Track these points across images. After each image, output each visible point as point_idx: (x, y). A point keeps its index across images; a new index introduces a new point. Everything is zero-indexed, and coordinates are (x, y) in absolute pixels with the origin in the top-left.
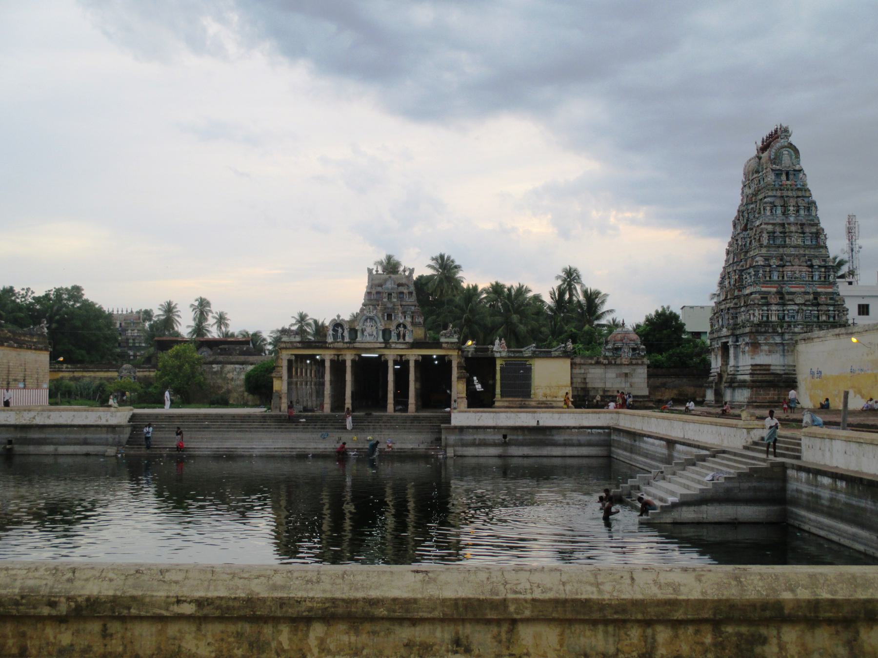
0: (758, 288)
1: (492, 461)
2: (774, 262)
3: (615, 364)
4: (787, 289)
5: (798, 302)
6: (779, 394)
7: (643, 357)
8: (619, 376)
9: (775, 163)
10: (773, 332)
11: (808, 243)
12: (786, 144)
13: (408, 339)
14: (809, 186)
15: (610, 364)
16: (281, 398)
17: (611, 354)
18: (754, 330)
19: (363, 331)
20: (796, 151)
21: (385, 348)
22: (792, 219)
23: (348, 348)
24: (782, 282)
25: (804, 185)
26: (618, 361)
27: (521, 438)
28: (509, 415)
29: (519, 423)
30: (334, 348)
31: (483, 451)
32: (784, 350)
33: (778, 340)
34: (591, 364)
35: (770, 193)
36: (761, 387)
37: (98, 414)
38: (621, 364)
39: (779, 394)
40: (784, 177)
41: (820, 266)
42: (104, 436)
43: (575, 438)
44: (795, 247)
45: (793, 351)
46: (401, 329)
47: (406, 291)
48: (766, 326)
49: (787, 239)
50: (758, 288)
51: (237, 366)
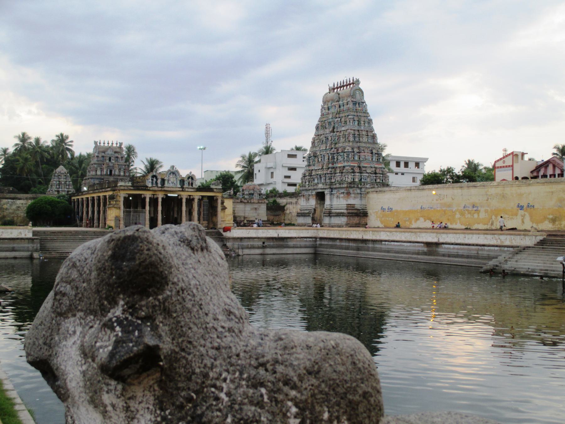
0: (349, 164)
2: (356, 150)
4: (362, 165)
11: (370, 141)
15: (248, 202)
19: (168, 181)
20: (362, 92)
21: (182, 191)
22: (362, 128)
23: (161, 191)
25: (366, 110)
26: (252, 201)
27: (272, 243)
28: (263, 231)
32: (361, 197)
33: (359, 191)
34: (238, 202)
36: (352, 216)
37: (20, 230)
40: (357, 105)
42: (26, 245)
43: (298, 243)
46: (190, 180)
47: (119, 156)
51: (10, 200)
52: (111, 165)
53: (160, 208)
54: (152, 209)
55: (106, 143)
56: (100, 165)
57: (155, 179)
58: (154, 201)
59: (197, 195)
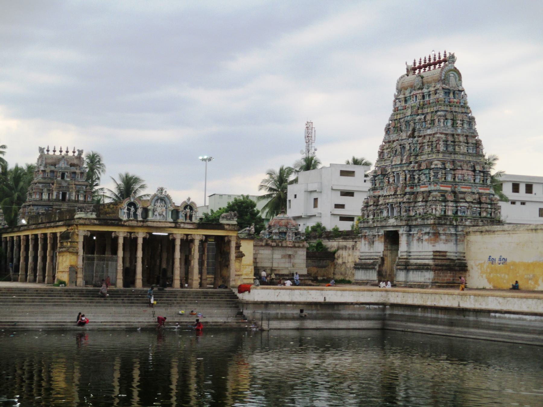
0: (438, 187)
1: (292, 333)
2: (449, 166)
3: (282, 246)
4: (459, 189)
5: (468, 200)
6: (453, 277)
7: (303, 241)
8: (284, 257)
9: (444, 83)
10: (450, 225)
12: (453, 68)
13: (194, 220)
14: (469, 105)
15: (277, 246)
16: (76, 273)
17: (277, 237)
18: (437, 222)
19: (154, 211)
20: (459, 75)
21: (175, 227)
22: (459, 131)
24: (454, 183)
25: (465, 103)
26: (284, 245)
28: (302, 291)
29: (310, 300)
30: (129, 226)
31: (284, 324)
32: (456, 240)
33: (453, 231)
34: (262, 246)
35: (443, 108)
36: (442, 270)
38: (286, 247)
39: (453, 277)
40: (451, 95)
41: (480, 171)
44: (463, 154)
45: (463, 241)
46: (188, 210)
47: (78, 171)
48: (445, 219)
49: (457, 147)
50: (438, 187)
52: (64, 184)
53: (140, 254)
54: (128, 255)
56: (47, 184)
57: (132, 209)
58: (130, 243)
59: (198, 234)
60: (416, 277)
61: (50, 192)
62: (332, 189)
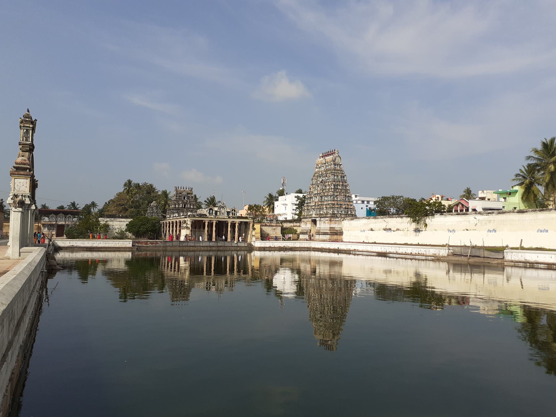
53: (214, 229)
54: (210, 229)
55: (185, 188)
56: (177, 200)
58: (210, 225)
59: (237, 221)
60: (322, 237)
61: (179, 205)
62: (449, 230)
